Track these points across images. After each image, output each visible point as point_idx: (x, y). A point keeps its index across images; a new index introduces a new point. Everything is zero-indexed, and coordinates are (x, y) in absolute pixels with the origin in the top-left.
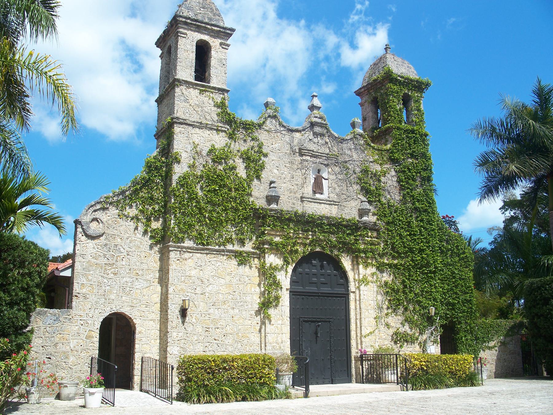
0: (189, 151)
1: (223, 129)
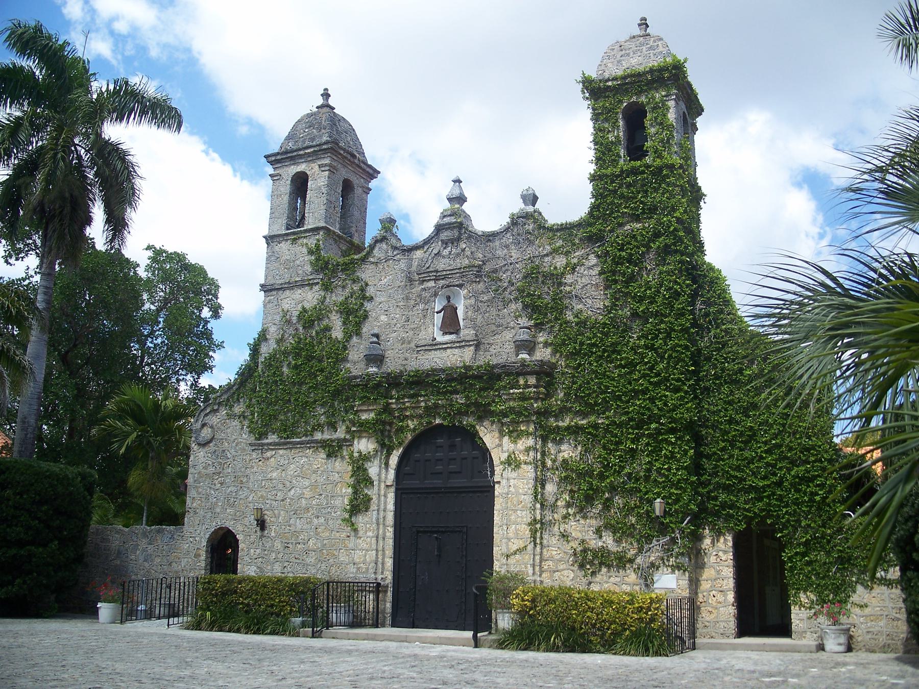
0: (277, 322)
1: (315, 281)
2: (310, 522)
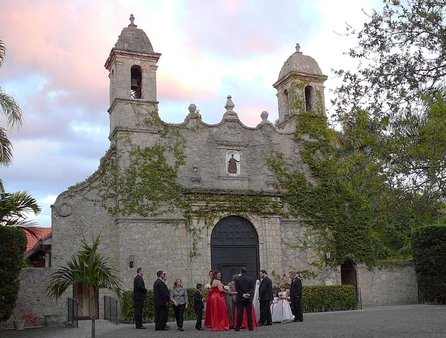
2: (163, 263)
